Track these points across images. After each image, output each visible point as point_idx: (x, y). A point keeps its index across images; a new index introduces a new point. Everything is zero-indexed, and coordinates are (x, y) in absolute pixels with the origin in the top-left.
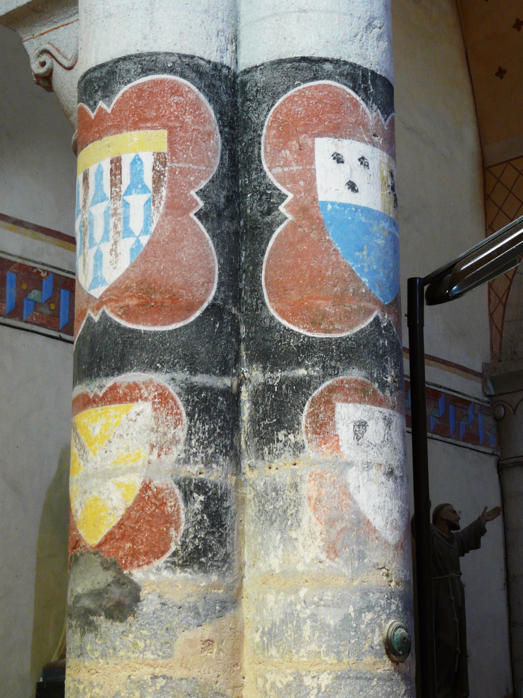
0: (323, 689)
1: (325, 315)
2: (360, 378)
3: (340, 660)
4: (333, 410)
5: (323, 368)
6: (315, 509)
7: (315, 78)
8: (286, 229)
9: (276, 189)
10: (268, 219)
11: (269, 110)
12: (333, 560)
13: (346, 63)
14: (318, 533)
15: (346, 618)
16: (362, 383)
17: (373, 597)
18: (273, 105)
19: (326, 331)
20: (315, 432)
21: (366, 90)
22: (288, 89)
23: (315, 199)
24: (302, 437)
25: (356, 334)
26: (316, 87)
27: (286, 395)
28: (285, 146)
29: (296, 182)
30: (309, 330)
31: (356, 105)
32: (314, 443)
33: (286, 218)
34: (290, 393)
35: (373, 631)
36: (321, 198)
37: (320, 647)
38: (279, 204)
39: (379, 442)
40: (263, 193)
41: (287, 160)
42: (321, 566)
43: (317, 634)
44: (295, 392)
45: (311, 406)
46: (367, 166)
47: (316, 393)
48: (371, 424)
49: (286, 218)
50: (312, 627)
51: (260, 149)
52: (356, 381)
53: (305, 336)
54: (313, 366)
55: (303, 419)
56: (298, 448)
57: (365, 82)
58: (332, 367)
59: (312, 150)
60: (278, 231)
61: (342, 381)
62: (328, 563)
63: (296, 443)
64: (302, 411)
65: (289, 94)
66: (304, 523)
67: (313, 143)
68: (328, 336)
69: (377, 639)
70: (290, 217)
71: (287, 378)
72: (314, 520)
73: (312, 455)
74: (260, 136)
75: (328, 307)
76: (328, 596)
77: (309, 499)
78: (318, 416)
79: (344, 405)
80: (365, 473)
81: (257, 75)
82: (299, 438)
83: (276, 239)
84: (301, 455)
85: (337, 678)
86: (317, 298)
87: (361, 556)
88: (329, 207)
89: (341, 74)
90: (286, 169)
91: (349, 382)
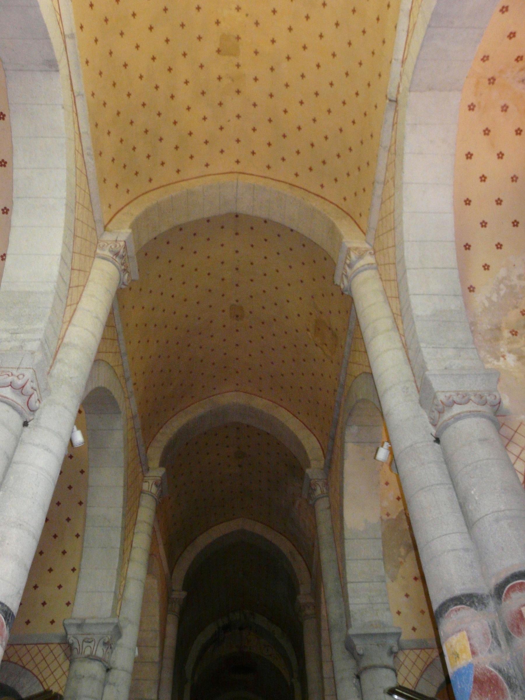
13: (6, 606)
31: (3, 626)
57: (9, 617)
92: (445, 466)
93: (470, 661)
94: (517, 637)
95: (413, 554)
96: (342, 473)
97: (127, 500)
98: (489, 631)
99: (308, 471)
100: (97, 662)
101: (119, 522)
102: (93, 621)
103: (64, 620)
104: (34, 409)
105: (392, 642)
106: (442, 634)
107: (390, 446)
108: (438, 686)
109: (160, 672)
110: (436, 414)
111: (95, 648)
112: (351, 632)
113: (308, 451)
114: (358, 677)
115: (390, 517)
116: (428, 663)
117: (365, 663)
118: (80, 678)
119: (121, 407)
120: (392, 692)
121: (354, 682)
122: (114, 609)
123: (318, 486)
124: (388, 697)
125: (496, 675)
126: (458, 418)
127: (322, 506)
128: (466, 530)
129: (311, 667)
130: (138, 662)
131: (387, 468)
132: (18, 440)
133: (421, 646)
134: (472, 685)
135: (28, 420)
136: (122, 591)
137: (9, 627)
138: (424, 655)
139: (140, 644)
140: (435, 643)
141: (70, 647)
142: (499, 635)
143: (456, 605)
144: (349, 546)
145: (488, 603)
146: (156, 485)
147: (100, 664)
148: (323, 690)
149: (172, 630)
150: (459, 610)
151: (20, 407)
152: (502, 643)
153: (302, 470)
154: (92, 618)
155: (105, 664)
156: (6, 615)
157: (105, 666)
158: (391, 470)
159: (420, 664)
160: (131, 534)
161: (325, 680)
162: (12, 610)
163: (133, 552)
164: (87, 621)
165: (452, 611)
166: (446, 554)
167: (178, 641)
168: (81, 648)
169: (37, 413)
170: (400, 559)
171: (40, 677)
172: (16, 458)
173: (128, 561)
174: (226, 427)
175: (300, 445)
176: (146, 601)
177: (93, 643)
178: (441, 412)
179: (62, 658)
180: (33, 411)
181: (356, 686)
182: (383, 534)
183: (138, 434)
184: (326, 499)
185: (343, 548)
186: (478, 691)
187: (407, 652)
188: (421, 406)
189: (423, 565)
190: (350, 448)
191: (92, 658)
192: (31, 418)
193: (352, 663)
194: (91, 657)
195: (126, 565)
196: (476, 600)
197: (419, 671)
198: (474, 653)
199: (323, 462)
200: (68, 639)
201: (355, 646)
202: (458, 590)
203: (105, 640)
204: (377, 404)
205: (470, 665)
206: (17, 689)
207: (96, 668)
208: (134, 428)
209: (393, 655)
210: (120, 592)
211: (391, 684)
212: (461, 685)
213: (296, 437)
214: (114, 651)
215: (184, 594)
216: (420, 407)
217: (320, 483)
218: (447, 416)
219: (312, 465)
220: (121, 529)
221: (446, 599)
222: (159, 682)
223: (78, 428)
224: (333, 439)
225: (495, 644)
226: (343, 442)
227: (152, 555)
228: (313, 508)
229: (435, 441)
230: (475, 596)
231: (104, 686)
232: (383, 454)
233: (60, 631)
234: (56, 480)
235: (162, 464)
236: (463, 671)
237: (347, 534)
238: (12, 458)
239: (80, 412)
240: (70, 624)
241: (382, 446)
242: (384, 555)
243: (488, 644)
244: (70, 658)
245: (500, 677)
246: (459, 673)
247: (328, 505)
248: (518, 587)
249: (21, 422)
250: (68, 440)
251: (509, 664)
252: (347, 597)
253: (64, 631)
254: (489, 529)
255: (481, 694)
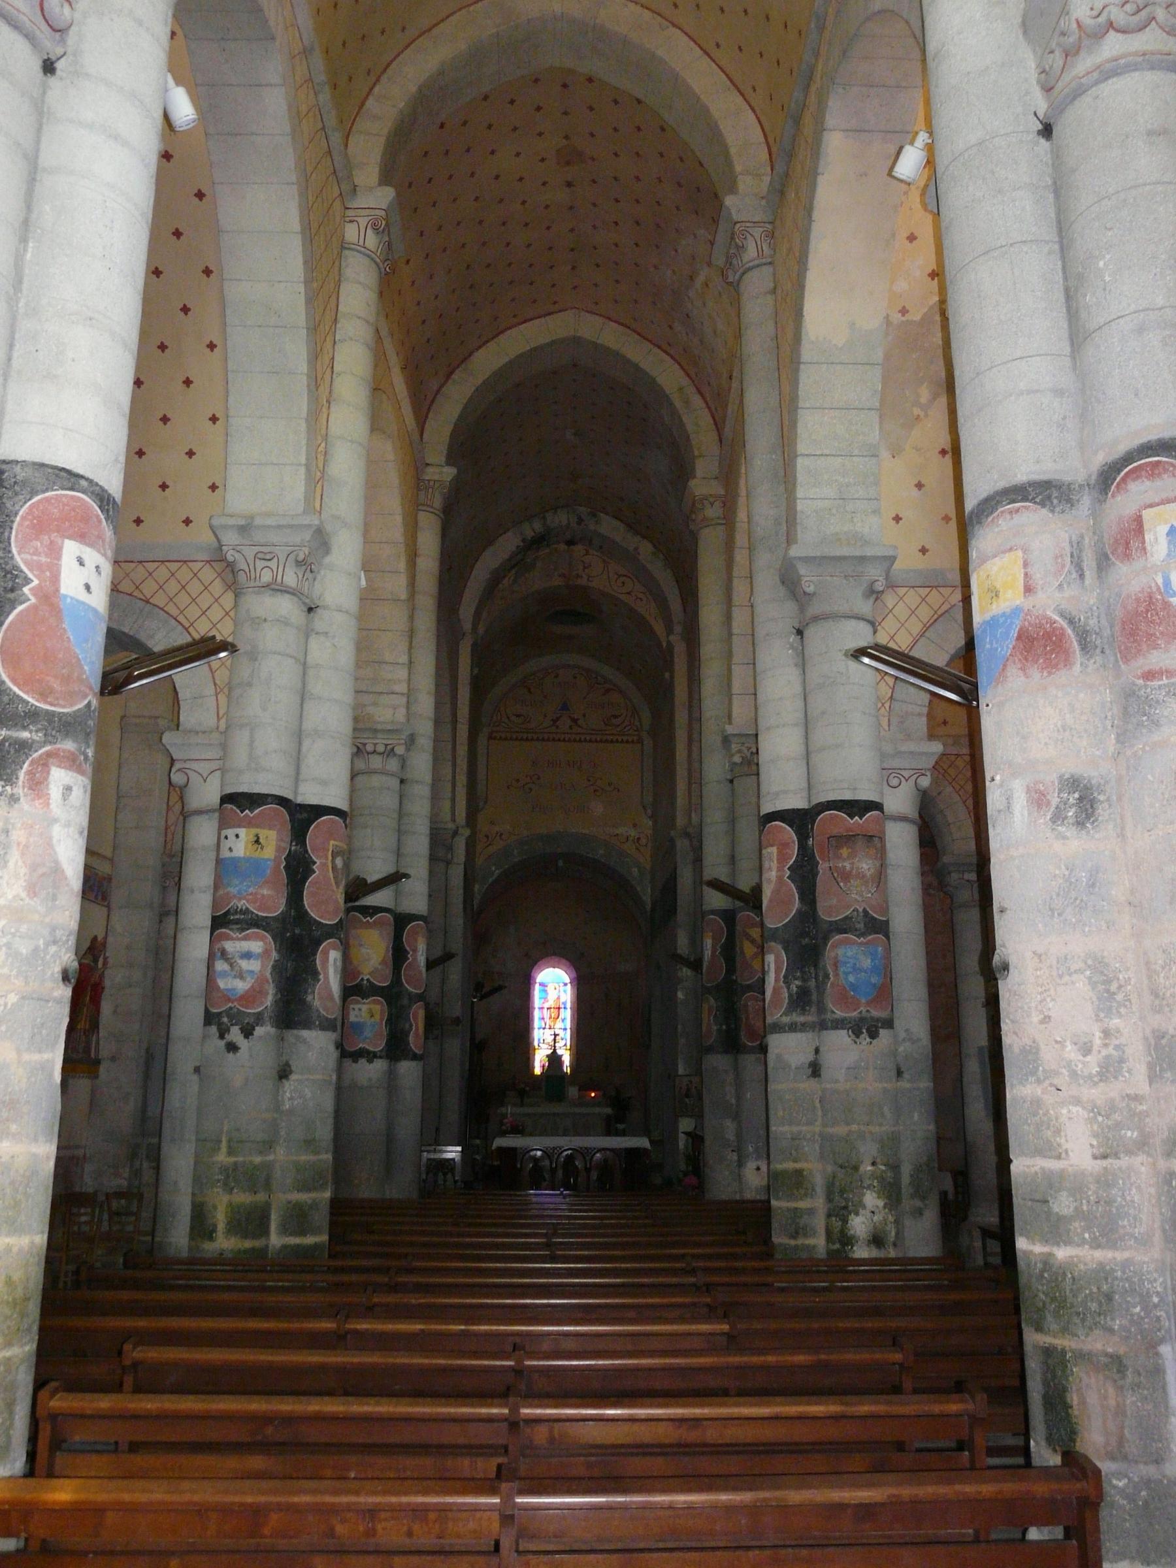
0: (9, 1006)
1: (52, 691)
2: (72, 749)
3: (27, 983)
4: (48, 773)
5: (45, 735)
6: (23, 854)
7: (72, 489)
8: (27, 610)
9: (22, 571)
10: (11, 596)
11: (25, 503)
12: (31, 898)
13: (97, 484)
14: (22, 875)
15: (36, 950)
16: (73, 754)
17: (59, 933)
18: (30, 499)
19: (51, 704)
20: (30, 788)
21: (108, 511)
22: (47, 490)
23: (57, 590)
24: (20, 790)
25: (74, 712)
26: (72, 497)
27: (9, 752)
28: (37, 539)
29: (43, 572)
30: (37, 701)
31: (100, 521)
32: (29, 798)
33: (29, 600)
34: (12, 751)
35: (55, 962)
36: (63, 591)
37: (11, 971)
38: (25, 586)
39: (78, 805)
40: (7, 572)
41: (37, 549)
42: (21, 903)
43: (10, 960)
44: (17, 751)
45: (30, 766)
46: (100, 573)
47: (35, 755)
48: (75, 789)
49: (29, 600)
50: (6, 954)
51: (11, 533)
52: (69, 751)
53: (32, 705)
54: (37, 731)
55: (22, 774)
56: (14, 799)
57: (108, 504)
58: (52, 736)
59: (61, 548)
60: (20, 608)
61: (59, 749)
62: (27, 900)
63: (12, 795)
64: (21, 768)
65: (47, 494)
66: (11, 865)
67: (63, 543)
68: (52, 708)
69: (57, 969)
70: (33, 600)
71: (11, 737)
72: (20, 863)
73: (26, 807)
74: (13, 522)
75: (56, 685)
76: (24, 928)
77: (19, 844)
78: (1118, 979)
79: (58, 769)
80: (66, 830)
81: (18, 469)
82: (15, 791)
83: (18, 615)
84: (16, 806)
85: (23, 998)
86: (47, 675)
87: (54, 898)
88: (69, 600)
89: (93, 493)
90: (35, 558)
91: (64, 751)
92: (1051, 196)
93: (1018, 602)
94: (1121, 565)
95: (943, 400)
96: (809, 210)
97: (311, 264)
98: (1068, 550)
99: (729, 201)
100: (287, 596)
101: (300, 318)
102: (270, 522)
103: (210, 519)
104: (61, 26)
105: (875, 573)
106: (974, 554)
107: (930, 141)
108: (952, 651)
109: (411, 618)
110: (1058, 59)
111: (281, 569)
112: (794, 552)
113: (733, 151)
114: (800, 632)
115: (908, 317)
116: (939, 613)
117: (814, 609)
118: (258, 622)
119: (272, 23)
120: (859, 653)
121: (791, 640)
122: (308, 498)
123: (750, 240)
124: (853, 664)
125: (1062, 629)
126: (1111, 71)
127: (756, 284)
128: (1068, 350)
129: (710, 615)
130: (368, 598)
131: (915, 197)
132: (41, 115)
133: (931, 581)
134: (1014, 643)
135: (53, 58)
136: (321, 465)
137: (112, 522)
138: (935, 598)
139: (368, 565)
140: (958, 578)
141: (231, 566)
142: (1085, 559)
143: (1014, 501)
144: (808, 379)
145: (1078, 501)
146: (375, 229)
147: (296, 599)
148: (730, 655)
149: (429, 542)
150: (1017, 511)
151: (25, 19)
152: (1087, 573)
153: (716, 199)
154: (268, 515)
155: (304, 598)
156: (101, 500)
157: (304, 603)
158: (925, 206)
159: (925, 613)
160: (329, 344)
161: (735, 639)
162: (111, 492)
163: (338, 381)
164: (258, 521)
165: (1002, 512)
166: (1013, 398)
167: (442, 562)
168: (252, 570)
169: (72, 38)
170: (916, 411)
171: (181, 618)
172: (45, 160)
173: (329, 402)
174: (536, 81)
175: (715, 135)
176: (372, 486)
177: (275, 560)
178: (1070, 53)
179: (217, 587)
180: (60, 31)
181: (792, 647)
182: (887, 357)
183: (321, 97)
184: (767, 271)
185: (795, 383)
186: (1021, 654)
187: (902, 591)
188: (1025, 33)
189: (961, 420)
190: (835, 144)
191: (276, 588)
192: (59, 51)
193: (790, 607)
194: (273, 586)
195: (324, 410)
196: (1055, 494)
197: (920, 626)
198: (1028, 590)
199: (767, 179)
200: (224, 552)
201: (799, 577)
202: (1022, 475)
203: (297, 556)
204: (916, 24)
205: (1017, 611)
206: (142, 637)
207: (286, 606)
208: (311, 79)
209: (874, 596)
210: (317, 465)
211: (861, 636)
212: (991, 644)
213: (706, 110)
214: (319, 577)
215: (449, 473)
216: (1021, 36)
217: (757, 232)
218: (1084, 64)
219: (741, 187)
220: (305, 331)
221: (996, 489)
222: (411, 633)
223: (178, 82)
224: (797, 121)
225: (1074, 575)
226: (820, 128)
227: (377, 389)
228: (735, 288)
229: (1039, 133)
230: (1055, 486)
231: (307, 637)
232: (910, 163)
233: (208, 538)
234: (151, 216)
235: (386, 178)
236: (1001, 620)
237: (806, 354)
238: (37, 157)
239: (173, 34)
240: (225, 527)
241: (912, 143)
242: (882, 401)
243: (1061, 575)
244: (235, 587)
245: (1069, 631)
246: (993, 623)
247: (772, 285)
248: (1147, 471)
249: (36, 65)
250: (161, 112)
251: (1091, 609)
252: (794, 485)
253: (213, 538)
254: (1119, 349)
255: (1026, 659)
